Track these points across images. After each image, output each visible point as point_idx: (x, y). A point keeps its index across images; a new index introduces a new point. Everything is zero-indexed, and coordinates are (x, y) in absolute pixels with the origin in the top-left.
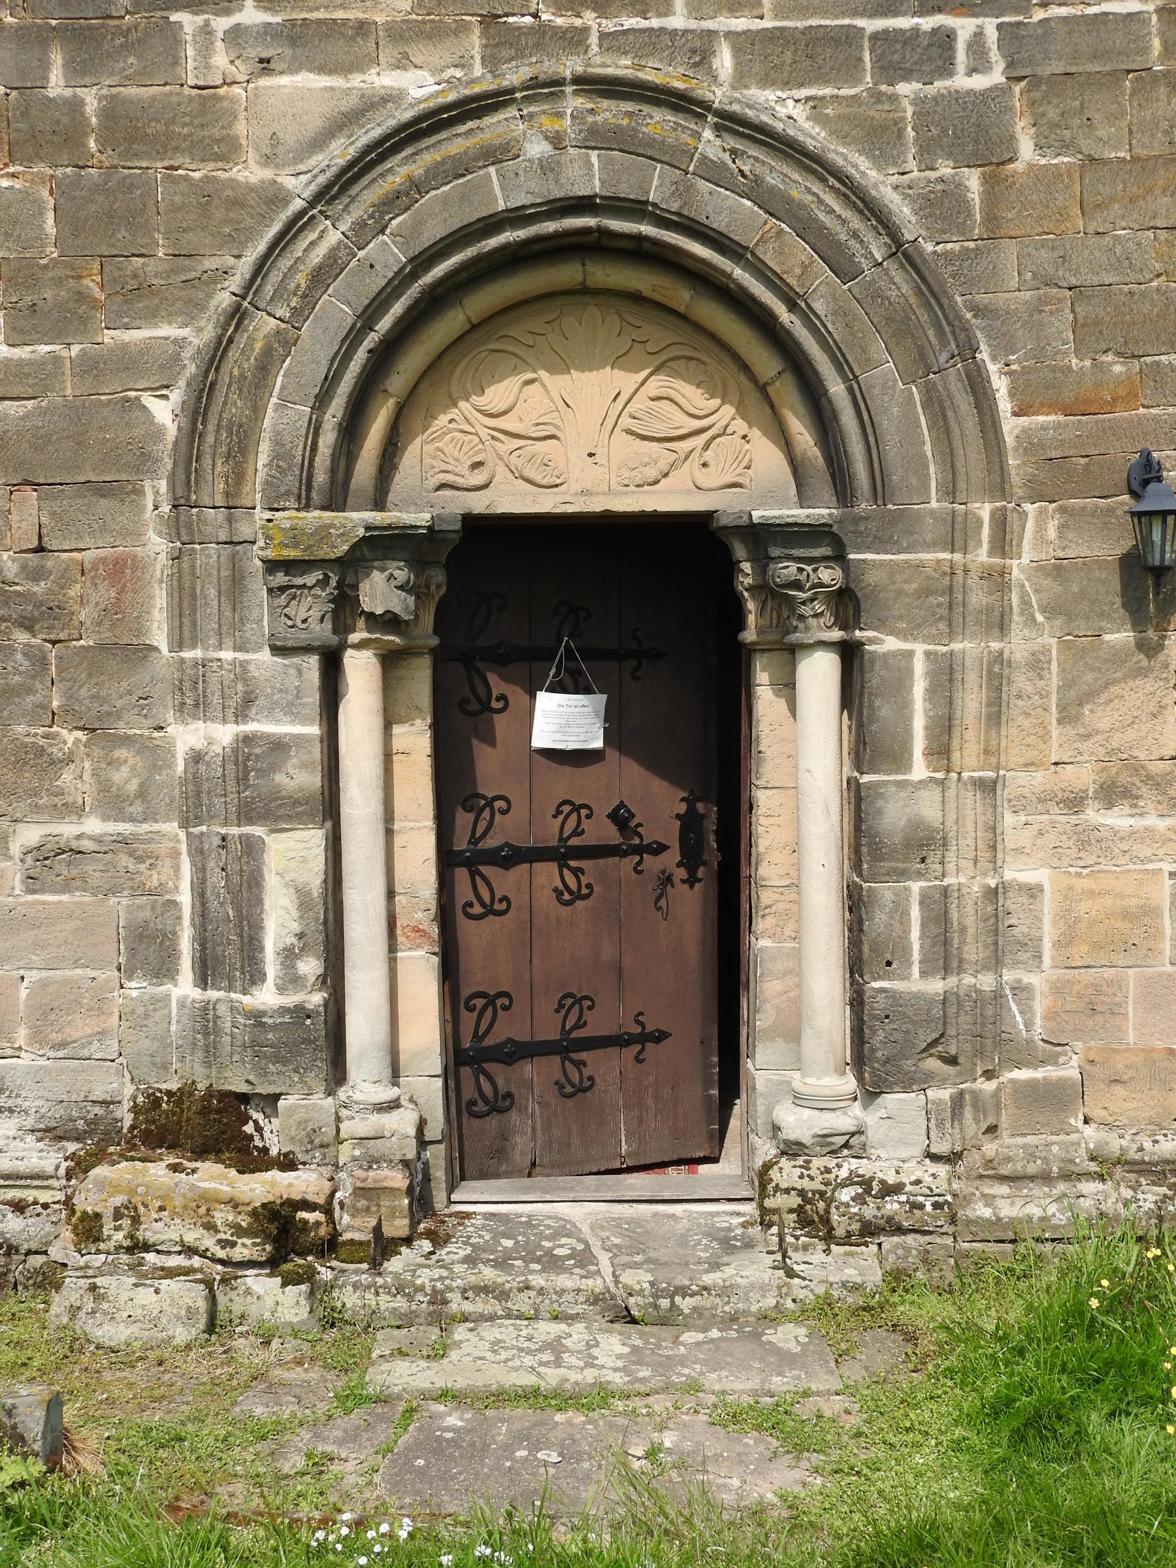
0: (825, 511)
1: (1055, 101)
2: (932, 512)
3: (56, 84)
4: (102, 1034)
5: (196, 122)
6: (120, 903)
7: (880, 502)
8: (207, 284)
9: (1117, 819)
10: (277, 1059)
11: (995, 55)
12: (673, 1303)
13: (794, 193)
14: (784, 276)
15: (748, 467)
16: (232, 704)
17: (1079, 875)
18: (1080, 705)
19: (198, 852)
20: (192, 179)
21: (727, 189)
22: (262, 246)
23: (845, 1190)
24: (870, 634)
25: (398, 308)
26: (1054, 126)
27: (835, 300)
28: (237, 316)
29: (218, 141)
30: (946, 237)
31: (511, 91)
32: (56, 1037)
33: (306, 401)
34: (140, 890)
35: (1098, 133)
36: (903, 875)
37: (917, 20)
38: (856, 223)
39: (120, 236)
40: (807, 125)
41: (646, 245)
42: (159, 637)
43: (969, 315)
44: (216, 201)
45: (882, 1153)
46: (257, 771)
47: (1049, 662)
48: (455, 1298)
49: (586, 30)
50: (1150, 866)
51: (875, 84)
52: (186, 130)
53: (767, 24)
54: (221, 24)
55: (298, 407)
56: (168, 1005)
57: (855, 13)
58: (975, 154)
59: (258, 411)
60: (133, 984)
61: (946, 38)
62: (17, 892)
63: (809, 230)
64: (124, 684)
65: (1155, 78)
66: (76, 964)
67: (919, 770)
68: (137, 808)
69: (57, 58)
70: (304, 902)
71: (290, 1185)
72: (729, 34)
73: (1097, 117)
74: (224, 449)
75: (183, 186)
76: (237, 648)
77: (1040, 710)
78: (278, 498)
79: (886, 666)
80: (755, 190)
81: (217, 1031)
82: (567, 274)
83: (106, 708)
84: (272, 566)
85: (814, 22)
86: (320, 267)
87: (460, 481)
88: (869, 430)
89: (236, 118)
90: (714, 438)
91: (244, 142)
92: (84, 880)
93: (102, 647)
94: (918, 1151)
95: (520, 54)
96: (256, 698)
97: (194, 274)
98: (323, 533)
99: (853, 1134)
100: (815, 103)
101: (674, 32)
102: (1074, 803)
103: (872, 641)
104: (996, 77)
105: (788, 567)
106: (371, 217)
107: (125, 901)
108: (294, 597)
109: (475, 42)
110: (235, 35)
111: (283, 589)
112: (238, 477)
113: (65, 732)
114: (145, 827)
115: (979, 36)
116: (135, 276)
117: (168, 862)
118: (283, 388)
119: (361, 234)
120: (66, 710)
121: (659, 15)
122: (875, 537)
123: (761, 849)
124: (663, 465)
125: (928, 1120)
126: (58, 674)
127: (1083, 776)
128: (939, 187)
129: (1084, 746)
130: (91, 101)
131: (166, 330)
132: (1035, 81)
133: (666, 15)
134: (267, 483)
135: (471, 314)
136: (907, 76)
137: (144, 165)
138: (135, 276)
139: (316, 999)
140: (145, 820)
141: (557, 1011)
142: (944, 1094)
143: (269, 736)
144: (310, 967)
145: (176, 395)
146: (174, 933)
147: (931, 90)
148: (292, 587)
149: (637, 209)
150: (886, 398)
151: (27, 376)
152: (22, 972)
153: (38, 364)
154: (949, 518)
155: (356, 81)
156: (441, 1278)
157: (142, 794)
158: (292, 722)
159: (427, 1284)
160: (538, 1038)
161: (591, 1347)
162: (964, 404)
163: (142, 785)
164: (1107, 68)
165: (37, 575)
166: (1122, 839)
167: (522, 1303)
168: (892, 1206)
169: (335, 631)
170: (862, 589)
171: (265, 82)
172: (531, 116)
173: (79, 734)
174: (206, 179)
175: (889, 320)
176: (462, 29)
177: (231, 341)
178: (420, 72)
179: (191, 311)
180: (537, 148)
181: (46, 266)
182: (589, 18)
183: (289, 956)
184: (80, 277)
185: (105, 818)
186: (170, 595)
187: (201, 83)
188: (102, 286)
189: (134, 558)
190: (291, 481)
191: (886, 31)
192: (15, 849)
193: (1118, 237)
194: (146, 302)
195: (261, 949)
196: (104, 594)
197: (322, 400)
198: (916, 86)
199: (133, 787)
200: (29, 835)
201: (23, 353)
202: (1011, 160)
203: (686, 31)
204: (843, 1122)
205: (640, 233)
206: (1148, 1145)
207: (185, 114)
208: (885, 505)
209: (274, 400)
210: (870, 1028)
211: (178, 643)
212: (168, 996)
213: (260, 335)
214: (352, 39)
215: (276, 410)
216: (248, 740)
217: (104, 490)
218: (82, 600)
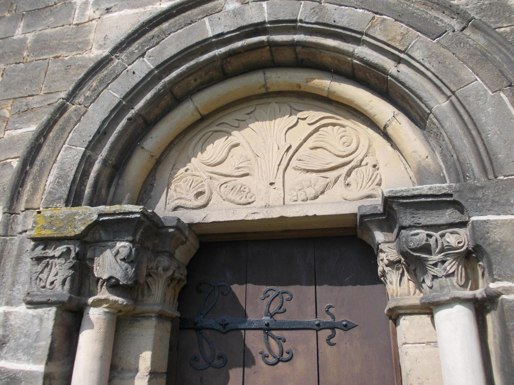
3: (18, 34)
5: (73, 37)
7: (491, 177)
14: (390, 42)
20: (65, 60)
21: (346, 6)
24: (506, 284)
27: (429, 49)
33: (82, 144)
39: (25, 88)
44: (73, 67)
52: (67, 41)
55: (78, 148)
84: (39, 241)
87: (189, 204)
88: (471, 127)
90: (353, 168)
91: (92, 41)
96: (9, 340)
98: (70, 219)
105: (417, 234)
108: (47, 266)
122: (493, 201)
124: (319, 187)
134: (50, 193)
135: (198, 105)
138: (27, 105)
148: (46, 258)
150: (481, 103)
170: (490, 244)
175: (472, 55)
190: (64, 191)
205: (294, 40)
208: (496, 177)
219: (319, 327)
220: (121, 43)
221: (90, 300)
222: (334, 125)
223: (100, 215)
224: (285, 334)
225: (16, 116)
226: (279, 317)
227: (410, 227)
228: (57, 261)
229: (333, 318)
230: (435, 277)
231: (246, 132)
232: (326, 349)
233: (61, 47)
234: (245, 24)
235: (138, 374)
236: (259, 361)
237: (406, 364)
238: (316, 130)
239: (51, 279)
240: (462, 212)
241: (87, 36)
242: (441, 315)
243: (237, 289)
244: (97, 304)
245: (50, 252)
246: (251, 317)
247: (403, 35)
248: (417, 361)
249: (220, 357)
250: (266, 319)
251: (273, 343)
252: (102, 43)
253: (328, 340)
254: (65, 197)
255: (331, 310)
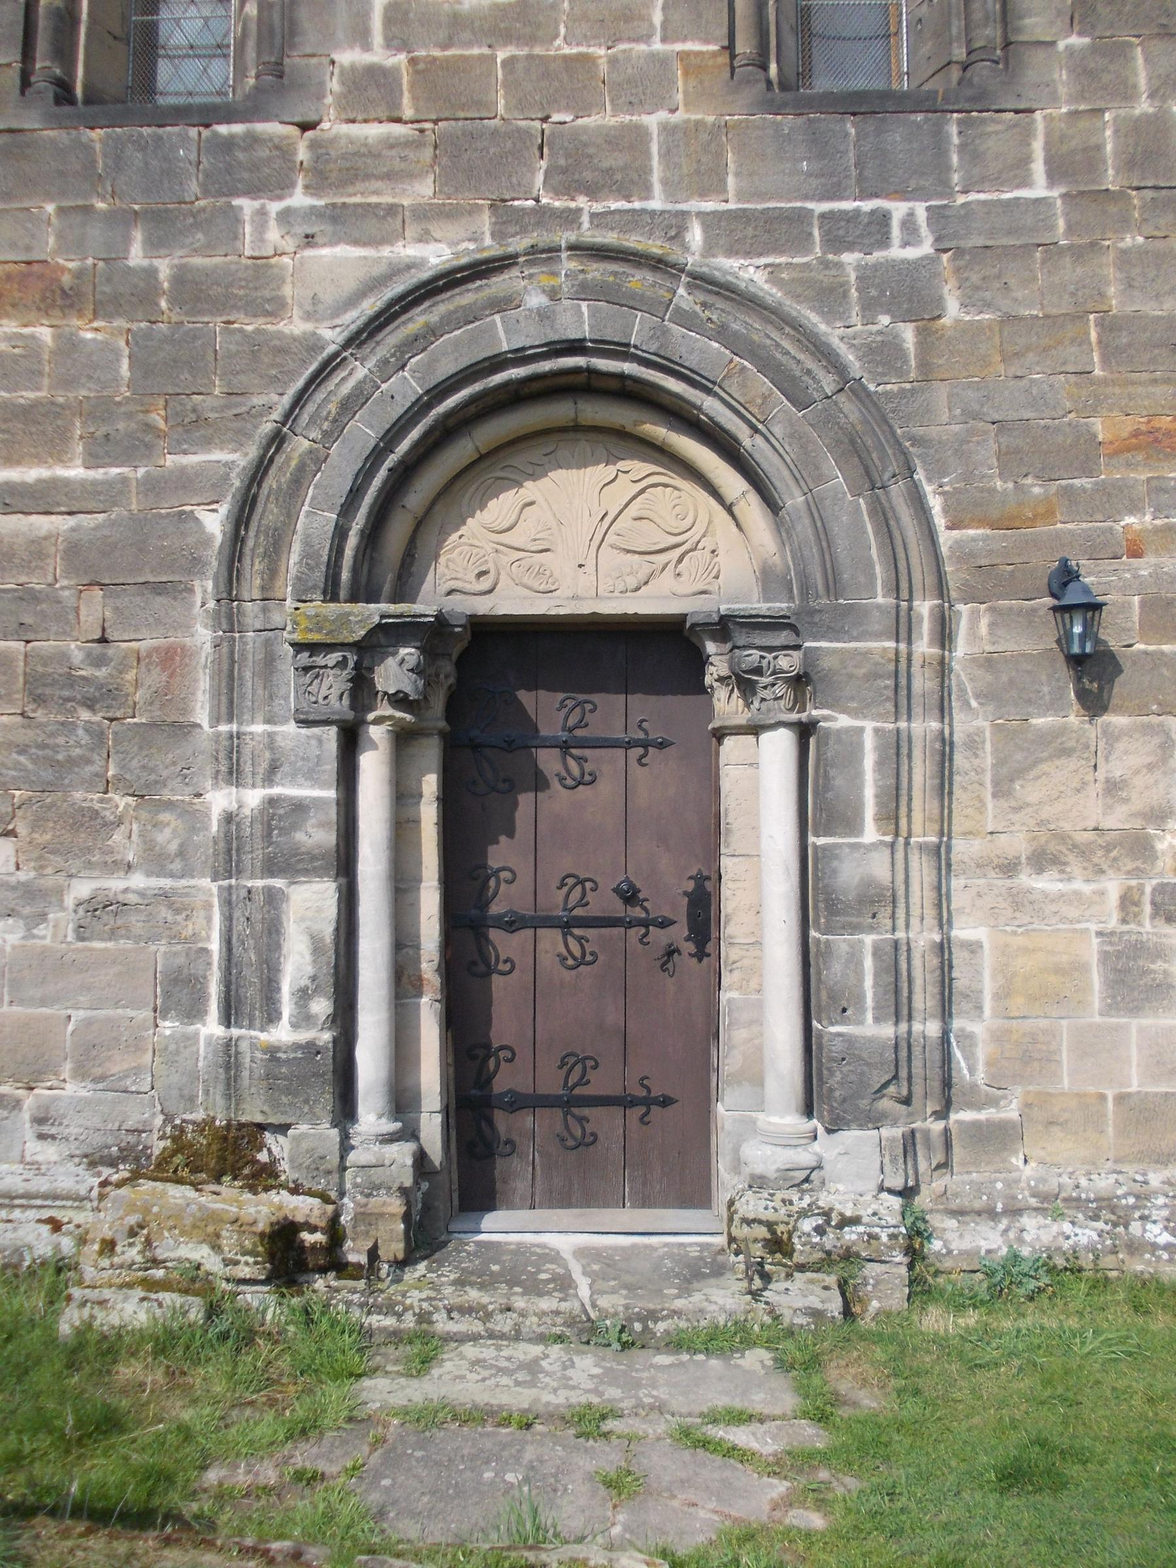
0: (784, 605)
1: (977, 268)
2: (878, 606)
3: (136, 256)
4: (137, 1070)
6: (161, 948)
8: (254, 417)
9: (1046, 883)
10: (288, 1091)
11: (924, 230)
12: (646, 1328)
13: (756, 338)
15: (717, 577)
16: (261, 771)
17: (1014, 933)
18: (1012, 781)
19: (228, 903)
22: (300, 383)
23: (807, 1221)
24: (825, 712)
25: (415, 434)
26: (977, 288)
27: (792, 425)
28: (277, 440)
29: (268, 301)
30: (886, 379)
31: (516, 256)
32: (98, 1071)
34: (175, 938)
35: (1014, 294)
36: (856, 928)
37: (857, 203)
38: (810, 364)
40: (766, 287)
41: (628, 383)
42: (202, 715)
43: (908, 444)
44: (265, 349)
45: (841, 1187)
46: (280, 829)
47: (984, 742)
48: (440, 1318)
49: (579, 211)
50: (1078, 926)
51: (824, 253)
53: (732, 206)
54: (274, 207)
56: (197, 1042)
57: (806, 198)
58: (909, 311)
59: (291, 516)
60: (167, 1024)
61: (883, 218)
62: (69, 939)
63: (767, 365)
64: (170, 756)
65: (1062, 251)
66: (117, 1005)
67: (870, 833)
68: (177, 866)
69: (138, 236)
70: (317, 949)
71: (296, 1208)
72: (700, 214)
73: (1012, 282)
74: (261, 550)
75: (238, 337)
76: (268, 721)
77: (976, 786)
78: (306, 591)
79: (839, 741)
80: (721, 334)
81: (238, 1066)
82: (560, 411)
83: (153, 777)
84: (299, 647)
85: (771, 205)
86: (348, 397)
87: (468, 587)
88: (822, 536)
89: (284, 282)
90: (686, 552)
91: (289, 301)
92: (127, 928)
93: (153, 725)
94: (873, 1186)
95: (524, 231)
97: (244, 409)
98: (343, 620)
99: (813, 1169)
100: (773, 269)
101: (652, 213)
102: (1009, 868)
103: (826, 718)
104: (926, 248)
106: (393, 355)
107: (163, 949)
109: (485, 221)
110: (286, 216)
111: (306, 669)
112: (272, 573)
113: (117, 798)
114: (184, 882)
115: (910, 217)
116: (194, 410)
117: (202, 913)
118: (313, 498)
119: (387, 369)
120: (119, 778)
121: (641, 199)
122: (829, 627)
123: (729, 910)
124: (642, 576)
125: (882, 1156)
126: (114, 746)
127: (1017, 844)
128: (879, 338)
129: (1015, 817)
130: (164, 268)
131: (218, 455)
132: (959, 252)
133: (647, 198)
134: (298, 578)
136: (850, 247)
137: (206, 319)
138: (194, 410)
139: (327, 1037)
140: (182, 877)
141: (561, 1067)
142: (898, 1132)
143: (291, 798)
144: (322, 1007)
145: (224, 508)
146: (205, 977)
147: (871, 259)
149: (621, 351)
151: (99, 493)
152: (69, 1012)
153: (109, 484)
154: (893, 612)
155: (386, 252)
156: (429, 1299)
157: (181, 853)
158: (312, 787)
159: (416, 1304)
160: (540, 1091)
161: (565, 1368)
162: (905, 514)
163: (181, 845)
164: (1018, 243)
165: (99, 661)
166: (1052, 901)
167: (503, 1324)
168: (851, 1235)
169: (353, 707)
171: (309, 253)
172: (531, 276)
173: (130, 799)
174: (258, 331)
176: (474, 210)
177: (271, 460)
178: (440, 245)
179: (238, 439)
180: (536, 300)
181: (120, 403)
182: (582, 202)
183: (303, 996)
184: (148, 411)
185: (149, 874)
186: (212, 678)
187: (256, 254)
188: (166, 420)
189: (183, 648)
190: (319, 576)
191: (832, 212)
192: (69, 901)
193: (1033, 381)
194: (203, 432)
195: (279, 990)
196: (155, 678)
197: (348, 509)
198: (857, 255)
199: (173, 847)
200: (82, 889)
201: (98, 474)
202: (939, 317)
203: (663, 212)
204: (804, 1157)
206: (1083, 1182)
207: (240, 279)
209: (306, 508)
210: (829, 1069)
211: (216, 720)
212: (196, 1034)
213: (296, 455)
214: (384, 218)
215: (307, 516)
216: (272, 802)
217: (159, 588)
218: (137, 684)
219: (629, 745)
220: (359, 332)
221: (371, 717)
222: (666, 486)
223: (382, 617)
224: (587, 752)
225: (180, 429)
226: (579, 733)
227: (745, 647)
228: (332, 672)
229: (647, 733)
230: (763, 700)
231: (544, 483)
232: (636, 771)
233: (232, 302)
234: (556, 338)
235: (423, 800)
236: (555, 784)
237: (725, 785)
238: (642, 491)
239: (323, 692)
240: (798, 635)
241: (279, 288)
242: (765, 737)
243: (524, 696)
244: (378, 721)
245: (320, 660)
246: (544, 732)
247: (765, 398)
248: (1041, 860)
249: (504, 781)
250: (564, 736)
251: (572, 763)
252: (309, 308)
253: (639, 760)
254: (322, 585)
255: (645, 725)
